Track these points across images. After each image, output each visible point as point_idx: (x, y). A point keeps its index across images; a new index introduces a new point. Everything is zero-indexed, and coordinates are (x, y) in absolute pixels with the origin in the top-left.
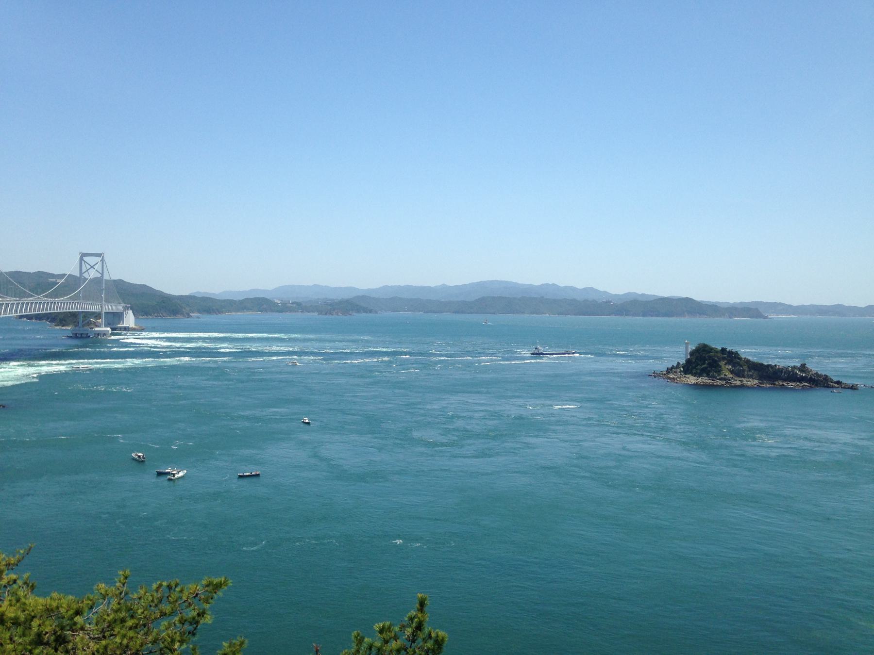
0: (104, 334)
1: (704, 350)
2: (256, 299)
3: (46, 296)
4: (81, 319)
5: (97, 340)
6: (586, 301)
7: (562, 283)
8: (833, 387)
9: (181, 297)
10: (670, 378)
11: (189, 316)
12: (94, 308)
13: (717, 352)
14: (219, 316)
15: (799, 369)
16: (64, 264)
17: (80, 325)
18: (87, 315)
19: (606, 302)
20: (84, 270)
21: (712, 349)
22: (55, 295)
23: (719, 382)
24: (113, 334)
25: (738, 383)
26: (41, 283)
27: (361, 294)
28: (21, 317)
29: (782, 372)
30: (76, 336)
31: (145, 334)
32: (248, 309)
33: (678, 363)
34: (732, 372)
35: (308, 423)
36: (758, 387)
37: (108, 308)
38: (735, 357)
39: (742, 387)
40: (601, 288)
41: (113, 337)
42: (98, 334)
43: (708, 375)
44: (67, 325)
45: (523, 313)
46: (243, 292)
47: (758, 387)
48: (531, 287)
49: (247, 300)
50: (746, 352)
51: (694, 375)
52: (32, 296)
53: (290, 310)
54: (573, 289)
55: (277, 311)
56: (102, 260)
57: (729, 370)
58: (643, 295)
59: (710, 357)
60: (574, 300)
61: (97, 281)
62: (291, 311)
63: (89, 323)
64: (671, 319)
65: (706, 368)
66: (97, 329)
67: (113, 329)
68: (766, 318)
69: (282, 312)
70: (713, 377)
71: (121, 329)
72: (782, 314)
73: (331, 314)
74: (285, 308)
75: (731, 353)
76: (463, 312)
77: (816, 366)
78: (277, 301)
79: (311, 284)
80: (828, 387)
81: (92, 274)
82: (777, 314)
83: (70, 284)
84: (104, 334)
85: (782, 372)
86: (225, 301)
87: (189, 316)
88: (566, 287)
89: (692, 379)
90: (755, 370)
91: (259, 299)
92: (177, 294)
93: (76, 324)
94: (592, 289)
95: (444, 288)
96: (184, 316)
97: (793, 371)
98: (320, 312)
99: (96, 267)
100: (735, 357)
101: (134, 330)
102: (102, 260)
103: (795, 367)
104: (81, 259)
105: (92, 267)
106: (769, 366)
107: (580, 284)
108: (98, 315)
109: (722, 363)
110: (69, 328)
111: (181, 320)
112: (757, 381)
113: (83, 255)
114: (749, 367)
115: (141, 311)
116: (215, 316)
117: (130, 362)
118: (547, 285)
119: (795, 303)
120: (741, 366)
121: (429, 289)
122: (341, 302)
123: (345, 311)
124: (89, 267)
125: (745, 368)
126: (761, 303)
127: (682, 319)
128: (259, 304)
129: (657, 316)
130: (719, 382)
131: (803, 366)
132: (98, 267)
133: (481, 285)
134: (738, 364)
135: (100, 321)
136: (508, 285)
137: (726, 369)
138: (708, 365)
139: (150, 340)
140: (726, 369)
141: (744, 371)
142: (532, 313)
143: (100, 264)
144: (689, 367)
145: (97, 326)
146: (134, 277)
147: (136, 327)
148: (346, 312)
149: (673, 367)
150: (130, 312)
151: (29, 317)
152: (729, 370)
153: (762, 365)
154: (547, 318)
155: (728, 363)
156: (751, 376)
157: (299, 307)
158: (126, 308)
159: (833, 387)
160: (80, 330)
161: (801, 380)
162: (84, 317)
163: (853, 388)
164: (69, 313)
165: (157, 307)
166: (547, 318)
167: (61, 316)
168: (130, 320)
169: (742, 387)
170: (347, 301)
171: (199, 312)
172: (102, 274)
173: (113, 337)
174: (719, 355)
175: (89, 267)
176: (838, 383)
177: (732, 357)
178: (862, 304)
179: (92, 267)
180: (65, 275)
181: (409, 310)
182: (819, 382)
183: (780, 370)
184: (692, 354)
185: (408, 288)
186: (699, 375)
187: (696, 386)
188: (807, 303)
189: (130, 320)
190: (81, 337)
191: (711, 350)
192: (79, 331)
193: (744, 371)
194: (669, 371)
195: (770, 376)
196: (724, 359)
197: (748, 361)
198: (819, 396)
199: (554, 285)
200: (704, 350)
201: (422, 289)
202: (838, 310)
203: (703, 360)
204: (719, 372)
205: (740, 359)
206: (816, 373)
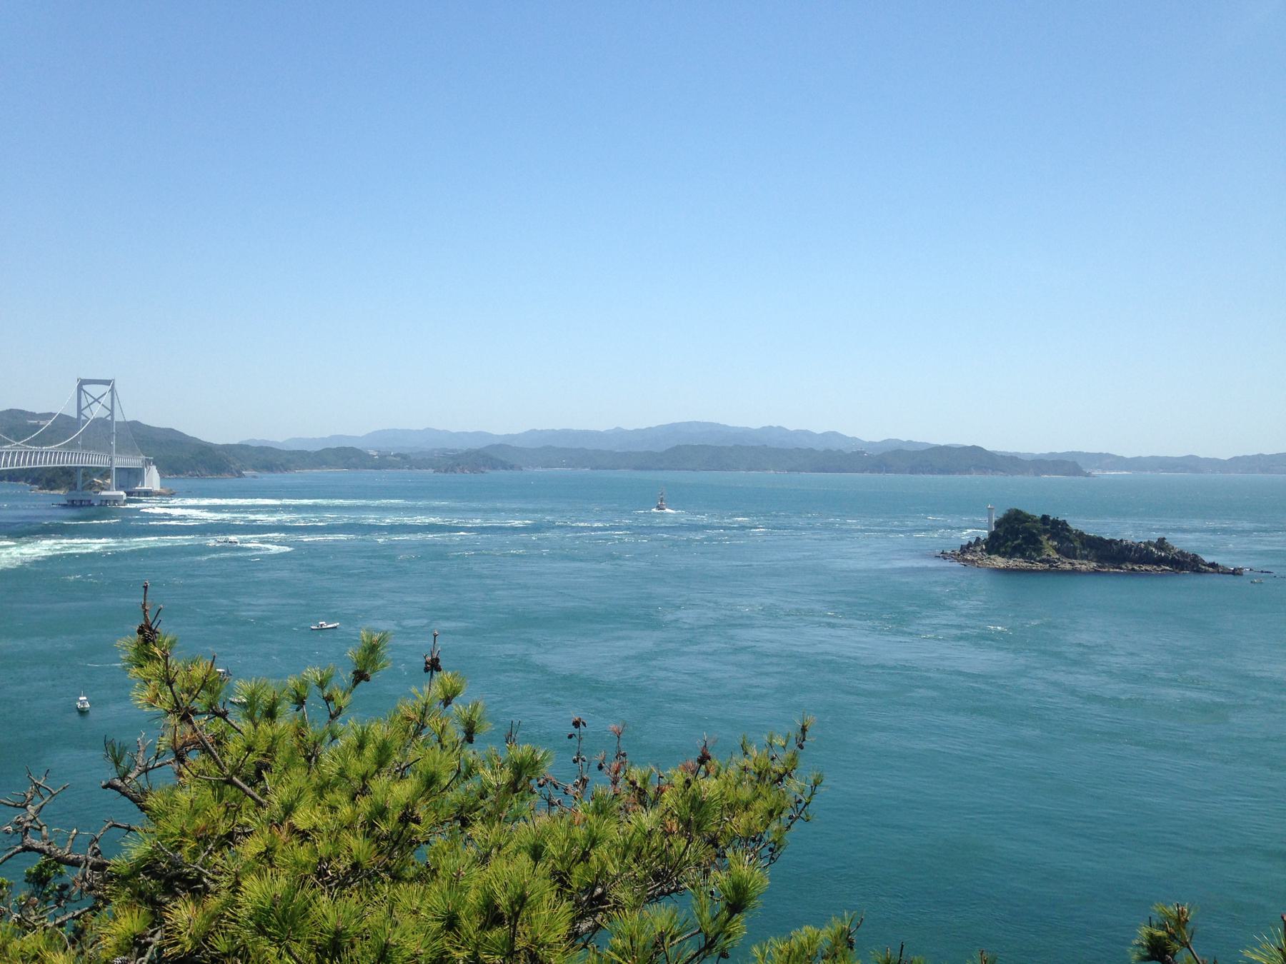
0: (116, 501)
1: (1016, 519)
2: (339, 449)
3: (28, 443)
4: (79, 479)
5: (106, 508)
6: (828, 451)
7: (791, 426)
8: (1206, 572)
10: (967, 560)
11: (240, 475)
12: (97, 460)
13: (1036, 522)
15: (1155, 546)
16: (53, 398)
17: (79, 487)
18: (89, 472)
19: (858, 452)
20: (84, 404)
21: (1028, 517)
22: (40, 441)
23: (1040, 566)
25: (1068, 567)
27: (497, 442)
29: (1130, 550)
30: (72, 504)
31: (176, 501)
32: (932, 470)
33: (978, 539)
34: (1058, 550)
35: (82, 712)
36: (1096, 572)
37: (121, 461)
38: (1063, 529)
39: (1075, 572)
40: (849, 433)
41: (129, 506)
42: (106, 500)
43: (1023, 556)
44: (59, 488)
45: (737, 469)
47: (1096, 572)
48: (746, 432)
49: (327, 450)
50: (1078, 523)
51: (1003, 555)
52: (9, 443)
54: (807, 433)
56: (112, 390)
57: (1054, 548)
58: (910, 442)
59: (1026, 529)
60: (812, 450)
61: (99, 422)
62: (394, 467)
63: (92, 486)
65: (1020, 545)
66: (104, 493)
67: (128, 494)
68: (1088, 475)
70: (1029, 559)
71: (139, 493)
72: (1111, 470)
73: (453, 470)
74: (383, 462)
75: (1056, 522)
76: (649, 468)
77: (1182, 542)
78: (372, 452)
80: (1199, 571)
81: (97, 411)
82: (1104, 470)
83: (61, 428)
84: (116, 501)
85: (1130, 550)
86: (293, 453)
87: (240, 475)
89: (1000, 562)
90: (1091, 547)
93: (72, 486)
94: (835, 433)
95: (619, 433)
96: (232, 474)
97: (1146, 548)
98: (438, 470)
99: (103, 400)
100: (1063, 529)
101: (159, 494)
102: (112, 390)
103: (1149, 543)
104: (80, 389)
105: (96, 400)
106: (1111, 541)
107: (818, 426)
108: (105, 473)
109: (1044, 538)
110: (61, 492)
111: (234, 482)
112: (482, 772)
113: (82, 383)
114: (1082, 543)
115: (169, 468)
116: (280, 475)
119: (1128, 455)
120: (1071, 542)
121: (598, 435)
122: (469, 453)
123: (474, 467)
124: (90, 400)
125: (1077, 544)
126: (1080, 454)
127: (968, 476)
128: (345, 457)
129: (932, 473)
130: (1040, 566)
131: (1162, 540)
132: (106, 400)
133: (673, 428)
134: (1068, 539)
135: (109, 481)
136: (713, 429)
137: (1049, 547)
138: (1022, 539)
139: (190, 509)
140: (1049, 547)
141: (1075, 549)
142: (749, 469)
143: (108, 396)
144: (995, 544)
145: (103, 489)
146: (156, 416)
147: (163, 491)
148: (475, 468)
149: (970, 544)
150: (154, 468)
152: (1054, 548)
153: (1101, 539)
154: (769, 477)
155: (1052, 537)
156: (1085, 557)
157: (405, 460)
158: (147, 463)
159: (1206, 572)
160: (78, 495)
161: (1159, 561)
162: (84, 475)
163: (1236, 572)
164: (68, 473)
165: (193, 462)
166: (769, 477)
168: (153, 479)
169: (1075, 572)
170: (477, 452)
171: (255, 468)
172: (112, 411)
173: (129, 506)
174: (1039, 525)
175: (90, 400)
176: (1213, 565)
177: (1057, 529)
178: (1225, 456)
179: (96, 400)
180: (51, 415)
182: (1186, 564)
183: (1128, 548)
184: (998, 524)
185: (566, 433)
186: (1009, 555)
187: (1006, 571)
188: (1145, 453)
189: (153, 479)
190: (81, 506)
191: (1028, 518)
192: (75, 495)
193: (1075, 549)
194: (966, 549)
195: (1112, 556)
196: (1045, 532)
197: (1082, 534)
198: (1189, 581)
199: (779, 427)
200: (1016, 519)
201: (586, 434)
202: (1189, 464)
203: (1016, 533)
204: (1039, 550)
205: (1069, 531)
206: (1181, 552)
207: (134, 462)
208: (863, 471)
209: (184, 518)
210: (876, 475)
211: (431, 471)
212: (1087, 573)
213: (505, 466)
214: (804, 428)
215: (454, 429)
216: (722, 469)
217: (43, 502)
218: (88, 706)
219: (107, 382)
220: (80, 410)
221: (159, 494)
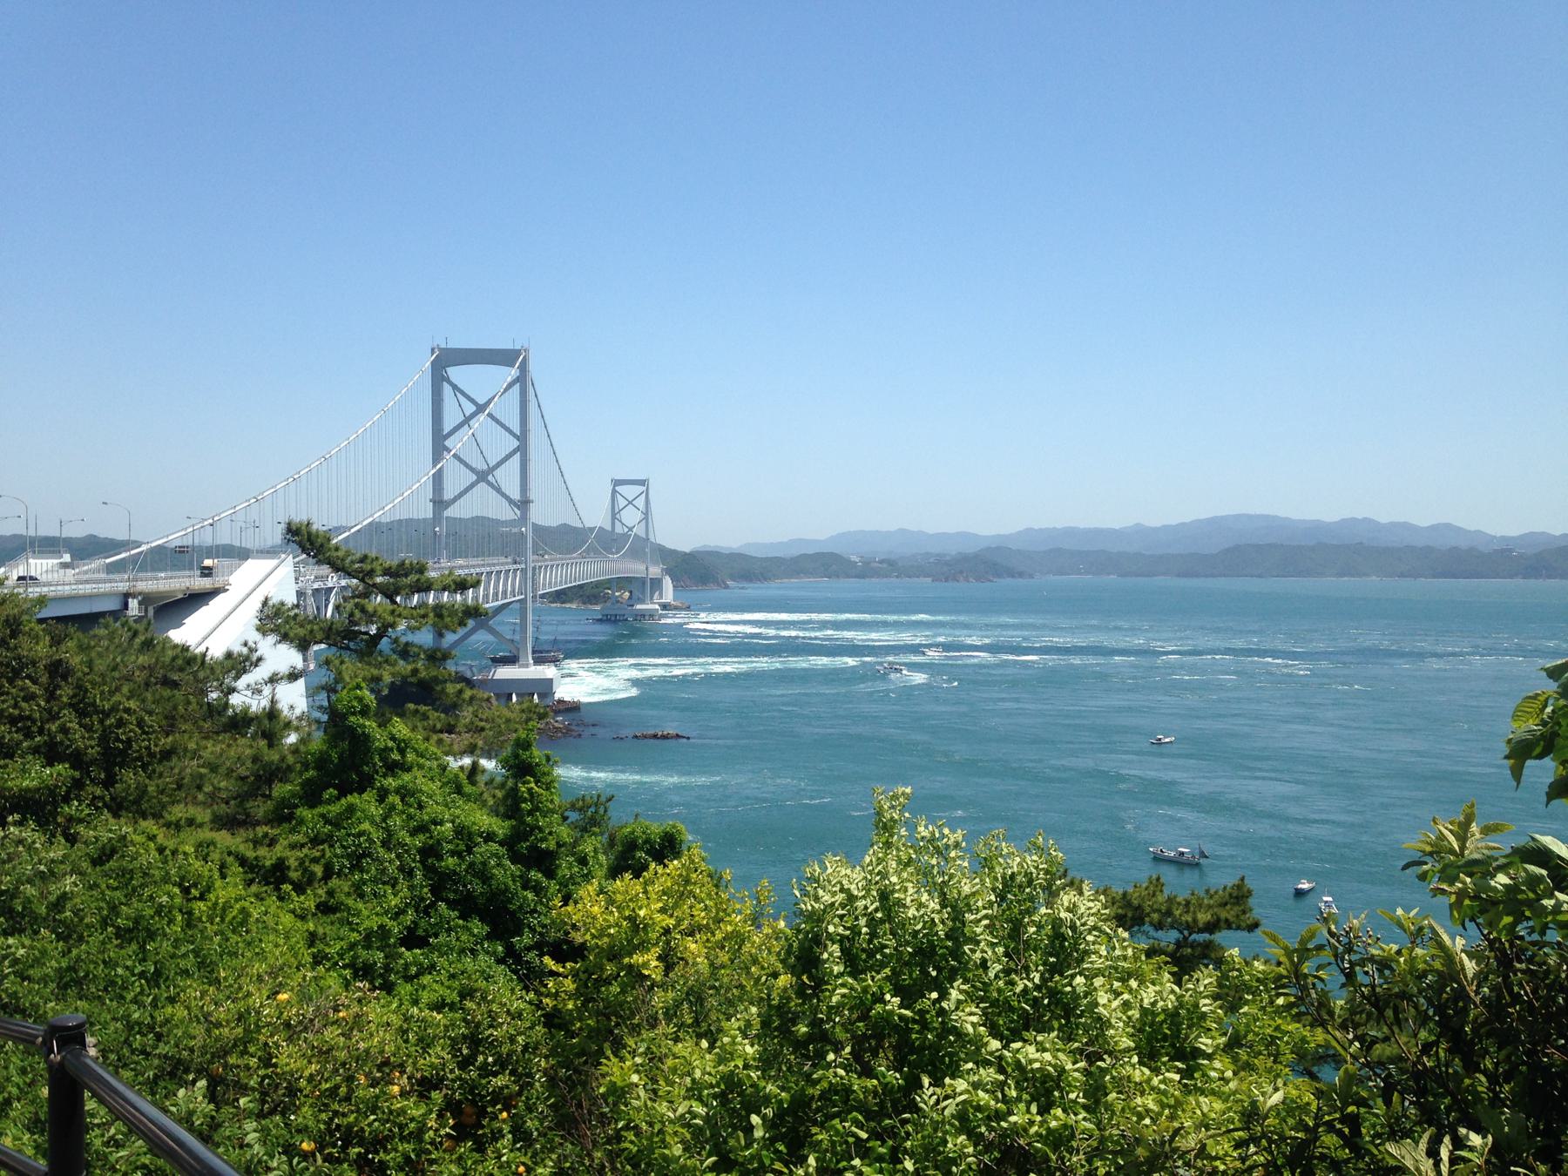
7: (1383, 518)
14: (766, 584)
19: (1503, 551)
20: (451, 419)
24: (666, 616)
27: (971, 549)
42: (642, 615)
44: (570, 601)
46: (1258, 516)
48: (1318, 527)
53: (876, 573)
55: (857, 576)
66: (639, 607)
74: (867, 569)
76: (1197, 575)
78: (854, 558)
79: (893, 527)
83: (607, 541)
87: (727, 587)
88: (1394, 525)
92: (1013, 531)
94: (1448, 526)
95: (1140, 531)
102: (522, 380)
104: (614, 492)
110: (598, 608)
111: (723, 593)
113: (444, 360)
118: (1354, 519)
123: (974, 574)
132: (640, 503)
165: (699, 572)
181: (1087, 573)
189: (668, 593)
201: (1098, 532)
207: (655, 571)
208: (1511, 577)
209: (714, 634)
210: (1532, 582)
211: (929, 580)
212: (48, 546)
213: (1012, 574)
214: (1359, 514)
215: (931, 528)
216: (1299, 574)
217: (577, 621)
218: (1335, 910)
219: (642, 483)
220: (439, 503)
221: (676, 608)
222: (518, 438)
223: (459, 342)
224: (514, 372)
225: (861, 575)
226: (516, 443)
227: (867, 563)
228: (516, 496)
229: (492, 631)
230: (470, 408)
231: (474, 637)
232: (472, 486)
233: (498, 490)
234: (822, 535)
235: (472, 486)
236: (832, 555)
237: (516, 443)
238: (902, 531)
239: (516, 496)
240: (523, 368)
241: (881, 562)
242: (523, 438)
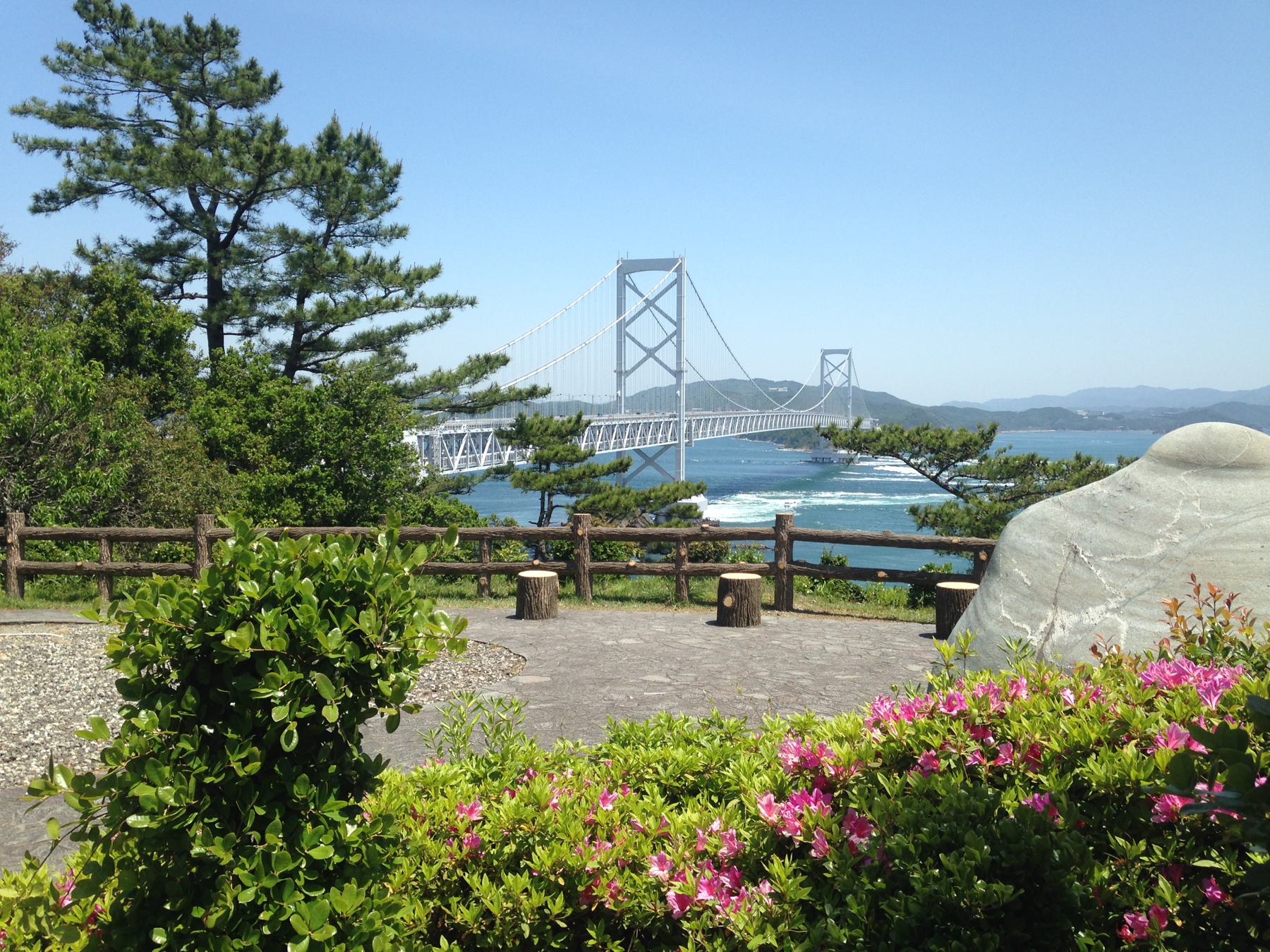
9: (935, 409)
20: (826, 373)
26: (763, 394)
28: (742, 436)
30: (815, 461)
41: (862, 464)
53: (1103, 426)
56: (849, 359)
64: (1261, 434)
69: (1089, 429)
78: (1080, 412)
81: (837, 380)
91: (1052, 409)
92: (929, 405)
102: (849, 359)
104: (823, 358)
113: (626, 269)
117: (876, 500)
132: (844, 368)
151: (752, 437)
167: (793, 435)
172: (849, 377)
175: (831, 368)
217: (793, 459)
219: (845, 352)
220: (621, 374)
222: (675, 324)
223: (635, 255)
224: (670, 276)
225: (1088, 427)
226: (671, 328)
227: (1093, 418)
228: (674, 368)
229: (658, 468)
230: (640, 303)
231: (644, 471)
232: (645, 359)
233: (661, 363)
234: (1233, 388)
235: (645, 359)
236: (1060, 409)
237: (671, 328)
238: (1142, 388)
239: (674, 368)
240: (679, 270)
241: (1106, 416)
242: (678, 323)
